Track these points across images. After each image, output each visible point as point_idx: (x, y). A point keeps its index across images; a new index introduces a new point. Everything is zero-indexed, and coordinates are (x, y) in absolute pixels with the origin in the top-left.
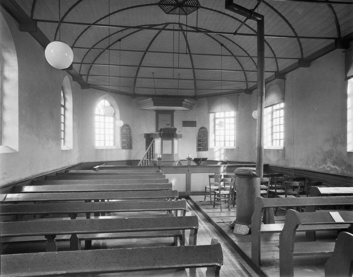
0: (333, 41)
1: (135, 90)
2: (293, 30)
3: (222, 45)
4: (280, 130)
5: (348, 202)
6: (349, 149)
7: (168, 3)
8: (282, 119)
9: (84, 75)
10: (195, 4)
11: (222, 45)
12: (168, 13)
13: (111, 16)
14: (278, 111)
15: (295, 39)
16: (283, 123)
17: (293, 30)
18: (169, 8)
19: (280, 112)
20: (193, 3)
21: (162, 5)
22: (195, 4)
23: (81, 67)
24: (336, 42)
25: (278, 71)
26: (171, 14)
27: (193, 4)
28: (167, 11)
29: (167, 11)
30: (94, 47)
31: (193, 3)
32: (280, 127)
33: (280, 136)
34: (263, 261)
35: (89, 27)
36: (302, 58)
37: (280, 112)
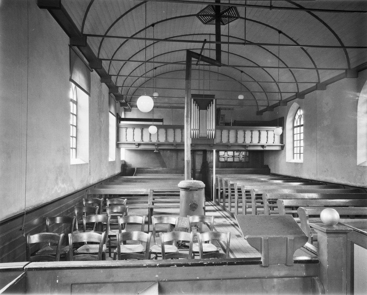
0: (344, 71)
1: (341, 238)
2: (339, 40)
3: (280, 32)
4: (300, 145)
5: (360, 209)
6: (360, 160)
7: (207, 14)
8: (302, 135)
9: (119, 87)
10: (234, 14)
11: (280, 32)
12: (206, 23)
13: (147, 29)
14: (299, 128)
15: (342, 49)
16: (121, 129)
17: (339, 40)
18: (206, 19)
19: (300, 129)
20: (233, 14)
21: (200, 15)
22: (234, 14)
23: (117, 79)
24: (346, 73)
25: (268, 106)
26: (209, 24)
27: (232, 14)
28: (205, 21)
29: (205, 21)
30: (131, 60)
31: (233, 14)
32: (300, 142)
33: (236, 137)
34: (219, 152)
35: (127, 40)
36: (319, 82)
37: (300, 129)
